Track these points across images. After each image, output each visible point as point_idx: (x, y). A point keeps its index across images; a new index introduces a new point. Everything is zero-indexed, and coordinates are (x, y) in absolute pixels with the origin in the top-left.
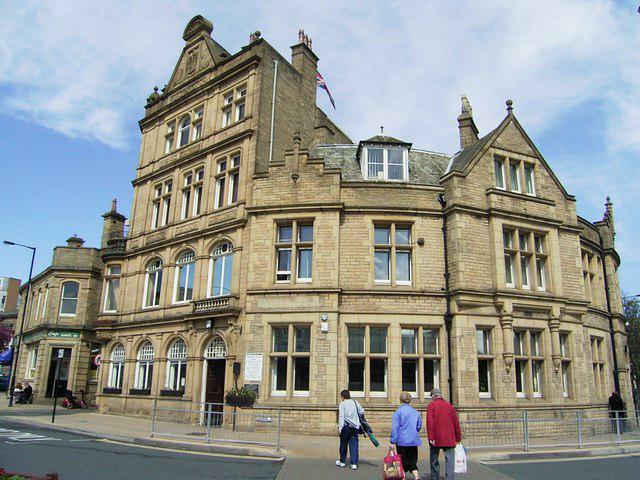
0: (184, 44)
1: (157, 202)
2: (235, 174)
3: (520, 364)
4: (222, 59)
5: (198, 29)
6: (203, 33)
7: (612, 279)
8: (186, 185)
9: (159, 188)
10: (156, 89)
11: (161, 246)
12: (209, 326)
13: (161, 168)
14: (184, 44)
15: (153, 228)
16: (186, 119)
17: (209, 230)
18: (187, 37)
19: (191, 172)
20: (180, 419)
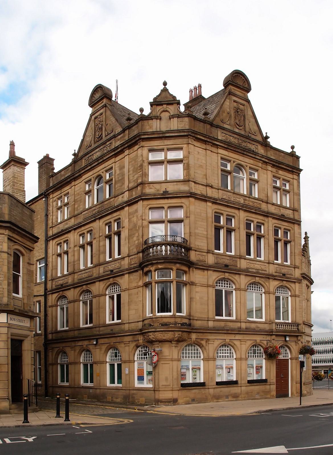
0: (90, 110)
1: (109, 237)
2: (118, 234)
3: (104, 371)
4: (126, 124)
5: (101, 97)
6: (105, 101)
7: (69, 347)
8: (107, 233)
9: (109, 224)
10: (75, 150)
11: (91, 281)
12: (95, 343)
13: (85, 219)
14: (90, 110)
15: (59, 275)
16: (99, 178)
17: (103, 276)
18: (92, 104)
19: (111, 222)
20: (265, 395)
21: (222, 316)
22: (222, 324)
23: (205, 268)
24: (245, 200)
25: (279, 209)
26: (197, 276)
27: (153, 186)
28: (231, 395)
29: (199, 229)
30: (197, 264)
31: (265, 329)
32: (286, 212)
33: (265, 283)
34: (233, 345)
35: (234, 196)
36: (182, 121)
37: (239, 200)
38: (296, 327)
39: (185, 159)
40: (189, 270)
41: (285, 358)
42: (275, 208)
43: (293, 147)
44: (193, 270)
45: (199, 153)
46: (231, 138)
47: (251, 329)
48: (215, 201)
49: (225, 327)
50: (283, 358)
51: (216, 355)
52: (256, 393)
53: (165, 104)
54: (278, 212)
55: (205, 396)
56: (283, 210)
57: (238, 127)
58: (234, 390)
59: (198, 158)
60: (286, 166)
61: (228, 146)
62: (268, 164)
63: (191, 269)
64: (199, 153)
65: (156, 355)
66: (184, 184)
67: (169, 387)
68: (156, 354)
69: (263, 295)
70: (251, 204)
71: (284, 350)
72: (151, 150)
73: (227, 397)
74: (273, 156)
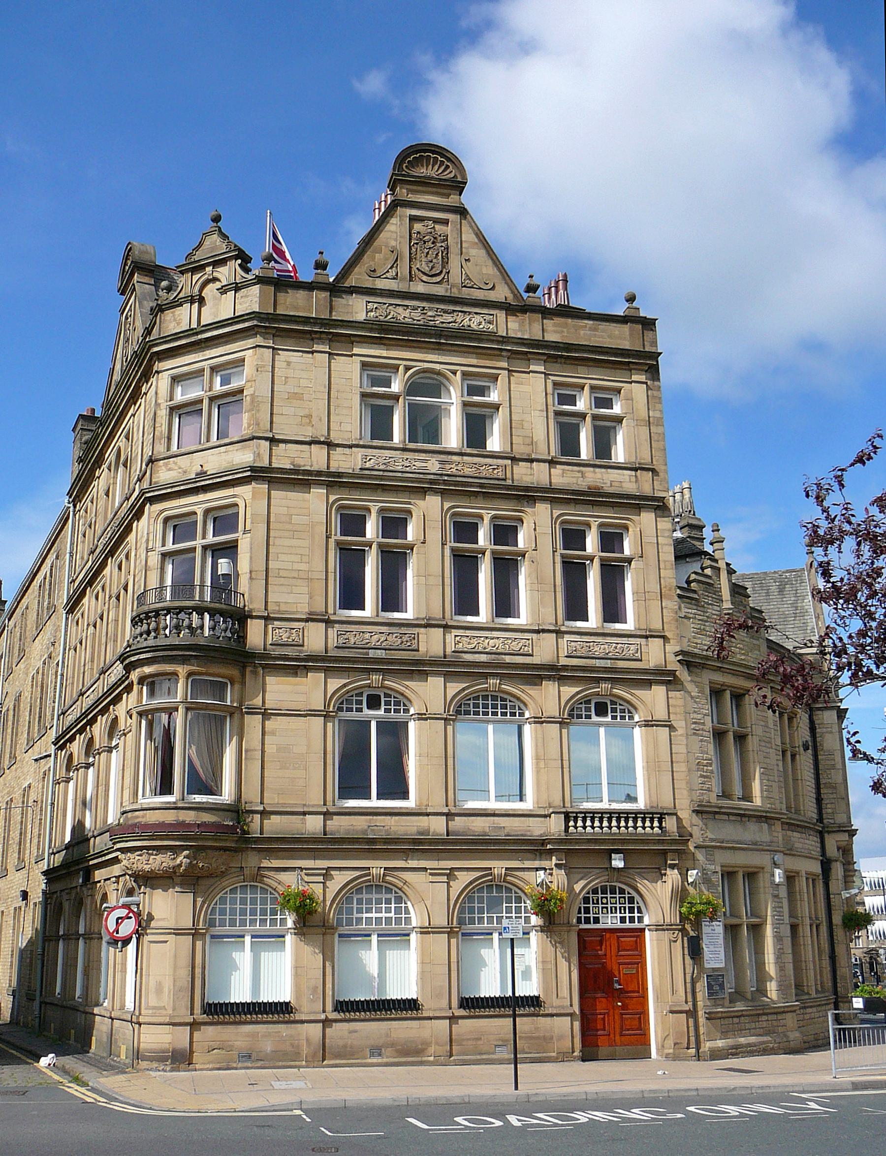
21: (368, 797)
22: (360, 823)
23: (298, 665)
24: (442, 462)
25: (579, 472)
26: (278, 690)
27: (175, 463)
28: (392, 1045)
29: (282, 557)
30: (265, 656)
31: (528, 833)
32: (605, 476)
33: (523, 691)
34: (400, 884)
35: (405, 457)
36: (246, 296)
37: (425, 465)
38: (656, 824)
39: (249, 384)
40: (243, 675)
41: (627, 925)
42: (563, 470)
43: (631, 299)
44: (255, 673)
45: (289, 363)
46: (400, 310)
47: (513, 833)
48: (333, 481)
49: (369, 831)
50: (620, 925)
51: (583, 905)
52: (496, 1043)
53: (208, 265)
54: (574, 480)
55: (292, 1045)
56: (595, 473)
57: (425, 278)
58: (403, 1029)
59: (286, 378)
60: (517, 344)
61: (384, 333)
62: (529, 356)
63: (249, 669)
64: (289, 363)
65: (131, 918)
66: (243, 448)
67: (164, 1012)
68: (131, 915)
69: (527, 729)
70: (468, 471)
71: (624, 898)
72: (176, 380)
73: (376, 1051)
74: (556, 332)
